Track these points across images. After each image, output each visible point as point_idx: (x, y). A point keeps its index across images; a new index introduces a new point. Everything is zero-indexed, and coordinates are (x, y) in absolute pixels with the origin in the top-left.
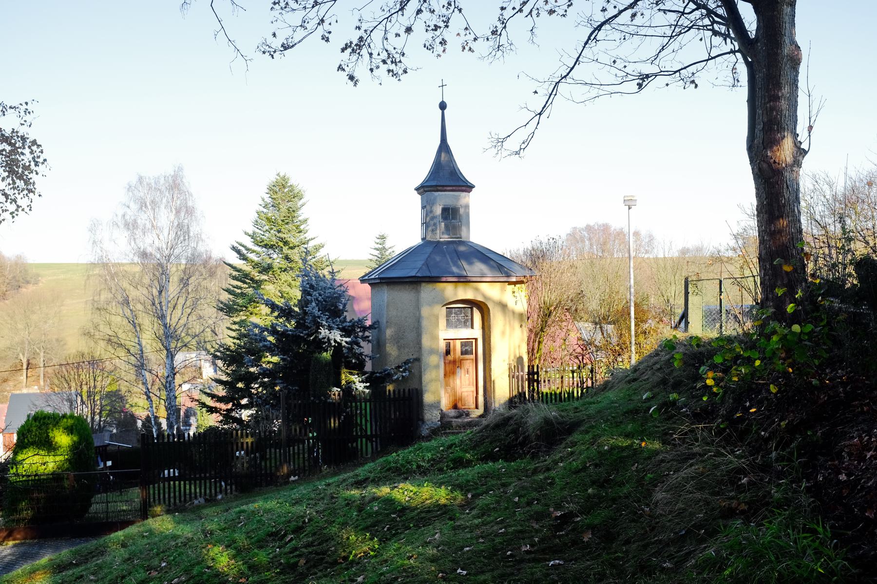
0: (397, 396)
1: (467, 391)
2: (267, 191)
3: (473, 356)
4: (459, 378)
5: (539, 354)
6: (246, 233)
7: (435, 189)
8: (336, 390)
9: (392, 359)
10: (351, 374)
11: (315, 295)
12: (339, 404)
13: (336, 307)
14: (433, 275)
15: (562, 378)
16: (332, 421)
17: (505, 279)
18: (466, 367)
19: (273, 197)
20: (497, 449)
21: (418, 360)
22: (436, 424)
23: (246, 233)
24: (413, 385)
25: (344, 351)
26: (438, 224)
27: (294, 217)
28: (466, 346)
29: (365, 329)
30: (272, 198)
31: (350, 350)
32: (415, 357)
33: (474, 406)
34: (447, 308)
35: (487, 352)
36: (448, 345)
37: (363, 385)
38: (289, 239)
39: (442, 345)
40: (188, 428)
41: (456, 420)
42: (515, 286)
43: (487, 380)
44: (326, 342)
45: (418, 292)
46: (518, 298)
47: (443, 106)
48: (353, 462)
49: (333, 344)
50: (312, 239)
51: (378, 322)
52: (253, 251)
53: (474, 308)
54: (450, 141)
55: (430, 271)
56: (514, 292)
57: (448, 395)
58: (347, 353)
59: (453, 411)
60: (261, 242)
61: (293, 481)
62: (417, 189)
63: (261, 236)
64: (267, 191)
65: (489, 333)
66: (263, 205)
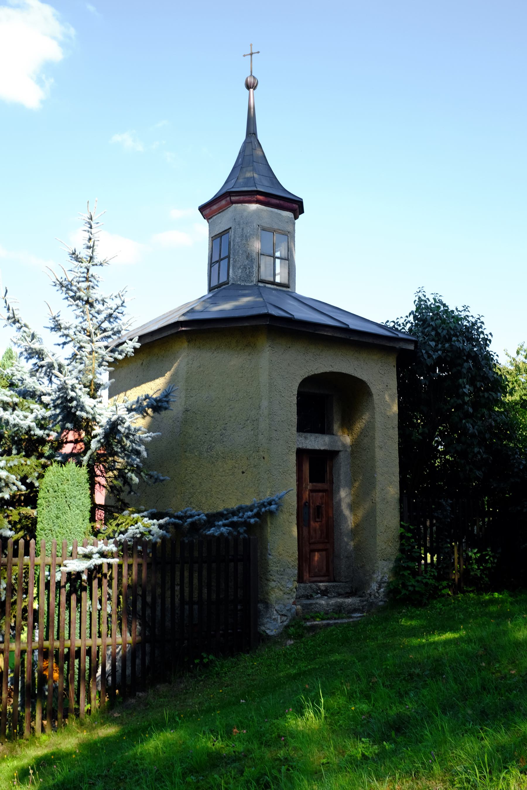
62: (202, 209)
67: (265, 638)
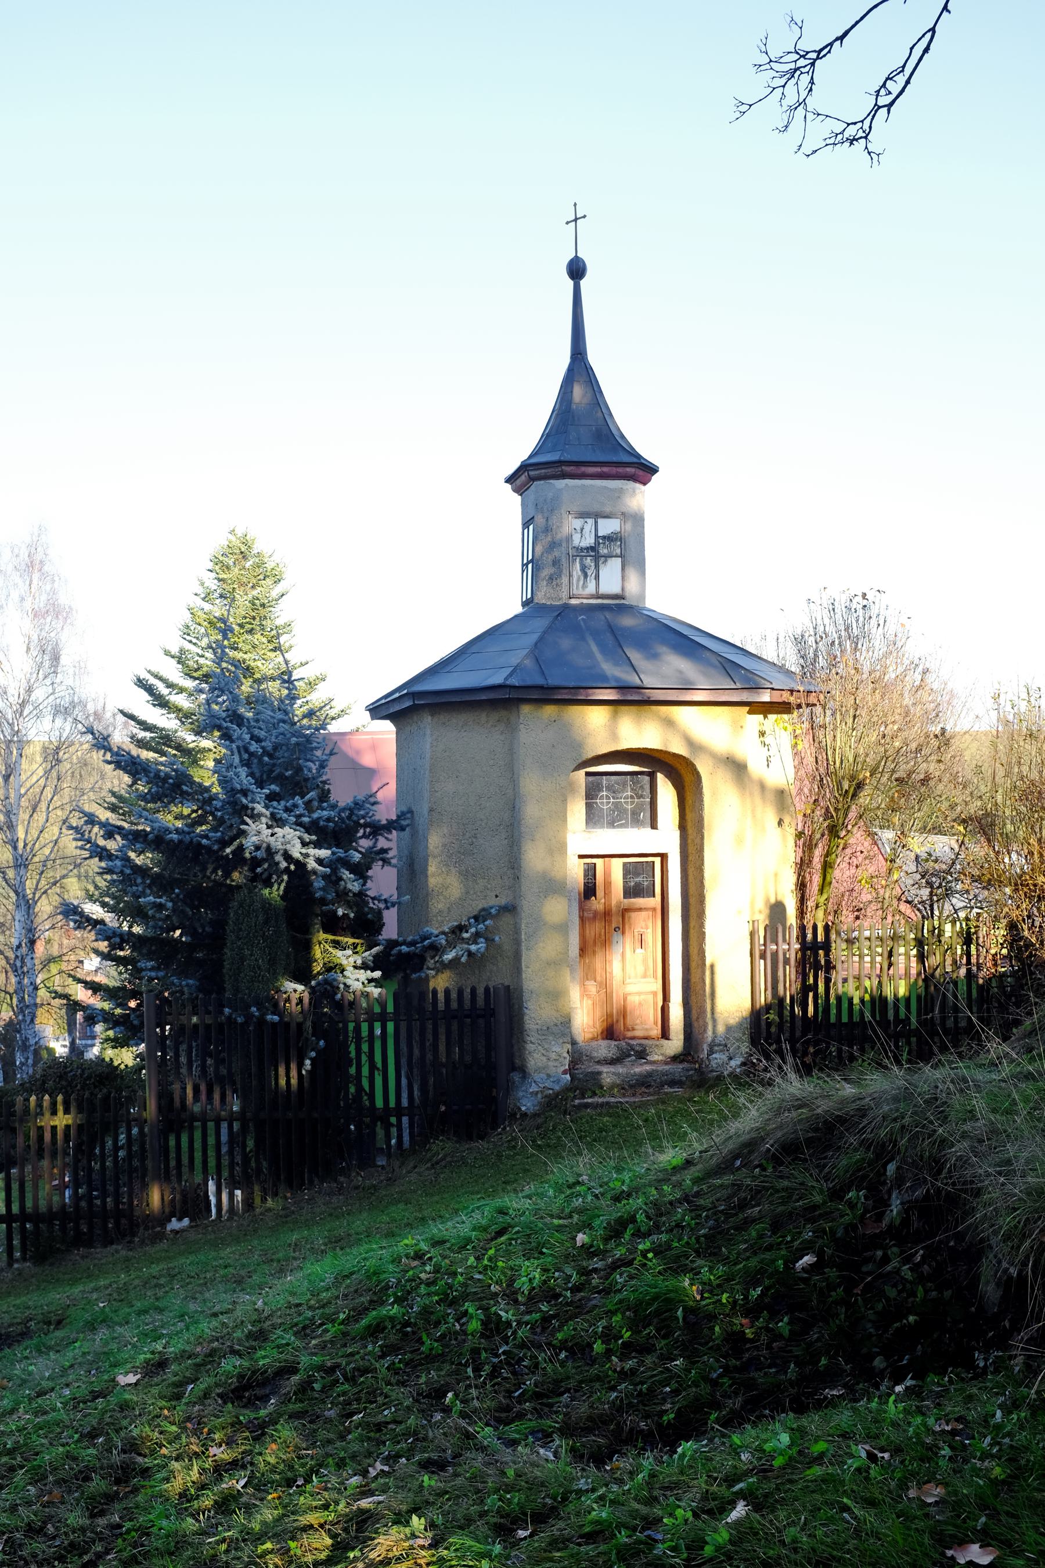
0: (454, 1005)
1: (639, 994)
2: (210, 566)
3: (656, 901)
4: (619, 957)
5: (825, 896)
6: (167, 653)
7: (557, 470)
8: (294, 989)
9: (437, 905)
10: (337, 945)
11: (240, 738)
12: (300, 1025)
13: (299, 770)
14: (552, 682)
15: (890, 954)
16: (282, 1071)
17: (745, 697)
18: (638, 930)
19: (221, 577)
20: (808, 1259)
21: (510, 909)
22: (558, 1081)
23: (167, 653)
24: (497, 976)
25: (316, 884)
26: (564, 561)
27: (265, 618)
28: (637, 875)
29: (377, 830)
30: (219, 580)
31: (333, 879)
32: (502, 901)
33: (656, 1031)
34: (588, 774)
35: (692, 889)
36: (590, 872)
37: (364, 975)
38: (252, 664)
39: (575, 871)
40: (89, 1042)
41: (612, 1069)
42: (765, 717)
43: (693, 965)
44: (264, 860)
45: (512, 729)
46: (773, 751)
47: (576, 270)
48: (336, 1181)
49: (284, 864)
50: (302, 665)
51: (410, 811)
52: (181, 690)
53: (660, 777)
54: (594, 357)
55: (543, 673)
56: (762, 734)
57: (590, 1002)
58: (323, 889)
59: (604, 1043)
60: (196, 670)
61: (176, 1232)
62: (510, 480)
63: (197, 658)
64: (210, 566)
65: (698, 841)
66: (203, 596)
67: (516, 1116)
